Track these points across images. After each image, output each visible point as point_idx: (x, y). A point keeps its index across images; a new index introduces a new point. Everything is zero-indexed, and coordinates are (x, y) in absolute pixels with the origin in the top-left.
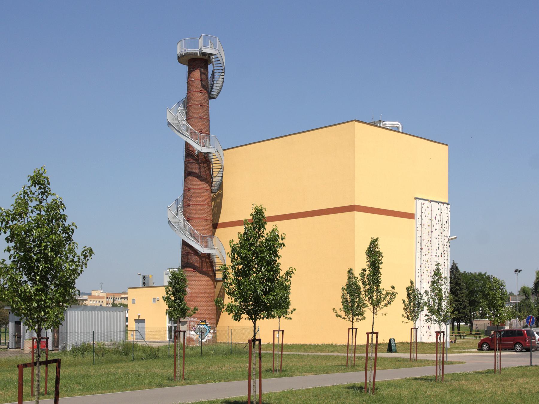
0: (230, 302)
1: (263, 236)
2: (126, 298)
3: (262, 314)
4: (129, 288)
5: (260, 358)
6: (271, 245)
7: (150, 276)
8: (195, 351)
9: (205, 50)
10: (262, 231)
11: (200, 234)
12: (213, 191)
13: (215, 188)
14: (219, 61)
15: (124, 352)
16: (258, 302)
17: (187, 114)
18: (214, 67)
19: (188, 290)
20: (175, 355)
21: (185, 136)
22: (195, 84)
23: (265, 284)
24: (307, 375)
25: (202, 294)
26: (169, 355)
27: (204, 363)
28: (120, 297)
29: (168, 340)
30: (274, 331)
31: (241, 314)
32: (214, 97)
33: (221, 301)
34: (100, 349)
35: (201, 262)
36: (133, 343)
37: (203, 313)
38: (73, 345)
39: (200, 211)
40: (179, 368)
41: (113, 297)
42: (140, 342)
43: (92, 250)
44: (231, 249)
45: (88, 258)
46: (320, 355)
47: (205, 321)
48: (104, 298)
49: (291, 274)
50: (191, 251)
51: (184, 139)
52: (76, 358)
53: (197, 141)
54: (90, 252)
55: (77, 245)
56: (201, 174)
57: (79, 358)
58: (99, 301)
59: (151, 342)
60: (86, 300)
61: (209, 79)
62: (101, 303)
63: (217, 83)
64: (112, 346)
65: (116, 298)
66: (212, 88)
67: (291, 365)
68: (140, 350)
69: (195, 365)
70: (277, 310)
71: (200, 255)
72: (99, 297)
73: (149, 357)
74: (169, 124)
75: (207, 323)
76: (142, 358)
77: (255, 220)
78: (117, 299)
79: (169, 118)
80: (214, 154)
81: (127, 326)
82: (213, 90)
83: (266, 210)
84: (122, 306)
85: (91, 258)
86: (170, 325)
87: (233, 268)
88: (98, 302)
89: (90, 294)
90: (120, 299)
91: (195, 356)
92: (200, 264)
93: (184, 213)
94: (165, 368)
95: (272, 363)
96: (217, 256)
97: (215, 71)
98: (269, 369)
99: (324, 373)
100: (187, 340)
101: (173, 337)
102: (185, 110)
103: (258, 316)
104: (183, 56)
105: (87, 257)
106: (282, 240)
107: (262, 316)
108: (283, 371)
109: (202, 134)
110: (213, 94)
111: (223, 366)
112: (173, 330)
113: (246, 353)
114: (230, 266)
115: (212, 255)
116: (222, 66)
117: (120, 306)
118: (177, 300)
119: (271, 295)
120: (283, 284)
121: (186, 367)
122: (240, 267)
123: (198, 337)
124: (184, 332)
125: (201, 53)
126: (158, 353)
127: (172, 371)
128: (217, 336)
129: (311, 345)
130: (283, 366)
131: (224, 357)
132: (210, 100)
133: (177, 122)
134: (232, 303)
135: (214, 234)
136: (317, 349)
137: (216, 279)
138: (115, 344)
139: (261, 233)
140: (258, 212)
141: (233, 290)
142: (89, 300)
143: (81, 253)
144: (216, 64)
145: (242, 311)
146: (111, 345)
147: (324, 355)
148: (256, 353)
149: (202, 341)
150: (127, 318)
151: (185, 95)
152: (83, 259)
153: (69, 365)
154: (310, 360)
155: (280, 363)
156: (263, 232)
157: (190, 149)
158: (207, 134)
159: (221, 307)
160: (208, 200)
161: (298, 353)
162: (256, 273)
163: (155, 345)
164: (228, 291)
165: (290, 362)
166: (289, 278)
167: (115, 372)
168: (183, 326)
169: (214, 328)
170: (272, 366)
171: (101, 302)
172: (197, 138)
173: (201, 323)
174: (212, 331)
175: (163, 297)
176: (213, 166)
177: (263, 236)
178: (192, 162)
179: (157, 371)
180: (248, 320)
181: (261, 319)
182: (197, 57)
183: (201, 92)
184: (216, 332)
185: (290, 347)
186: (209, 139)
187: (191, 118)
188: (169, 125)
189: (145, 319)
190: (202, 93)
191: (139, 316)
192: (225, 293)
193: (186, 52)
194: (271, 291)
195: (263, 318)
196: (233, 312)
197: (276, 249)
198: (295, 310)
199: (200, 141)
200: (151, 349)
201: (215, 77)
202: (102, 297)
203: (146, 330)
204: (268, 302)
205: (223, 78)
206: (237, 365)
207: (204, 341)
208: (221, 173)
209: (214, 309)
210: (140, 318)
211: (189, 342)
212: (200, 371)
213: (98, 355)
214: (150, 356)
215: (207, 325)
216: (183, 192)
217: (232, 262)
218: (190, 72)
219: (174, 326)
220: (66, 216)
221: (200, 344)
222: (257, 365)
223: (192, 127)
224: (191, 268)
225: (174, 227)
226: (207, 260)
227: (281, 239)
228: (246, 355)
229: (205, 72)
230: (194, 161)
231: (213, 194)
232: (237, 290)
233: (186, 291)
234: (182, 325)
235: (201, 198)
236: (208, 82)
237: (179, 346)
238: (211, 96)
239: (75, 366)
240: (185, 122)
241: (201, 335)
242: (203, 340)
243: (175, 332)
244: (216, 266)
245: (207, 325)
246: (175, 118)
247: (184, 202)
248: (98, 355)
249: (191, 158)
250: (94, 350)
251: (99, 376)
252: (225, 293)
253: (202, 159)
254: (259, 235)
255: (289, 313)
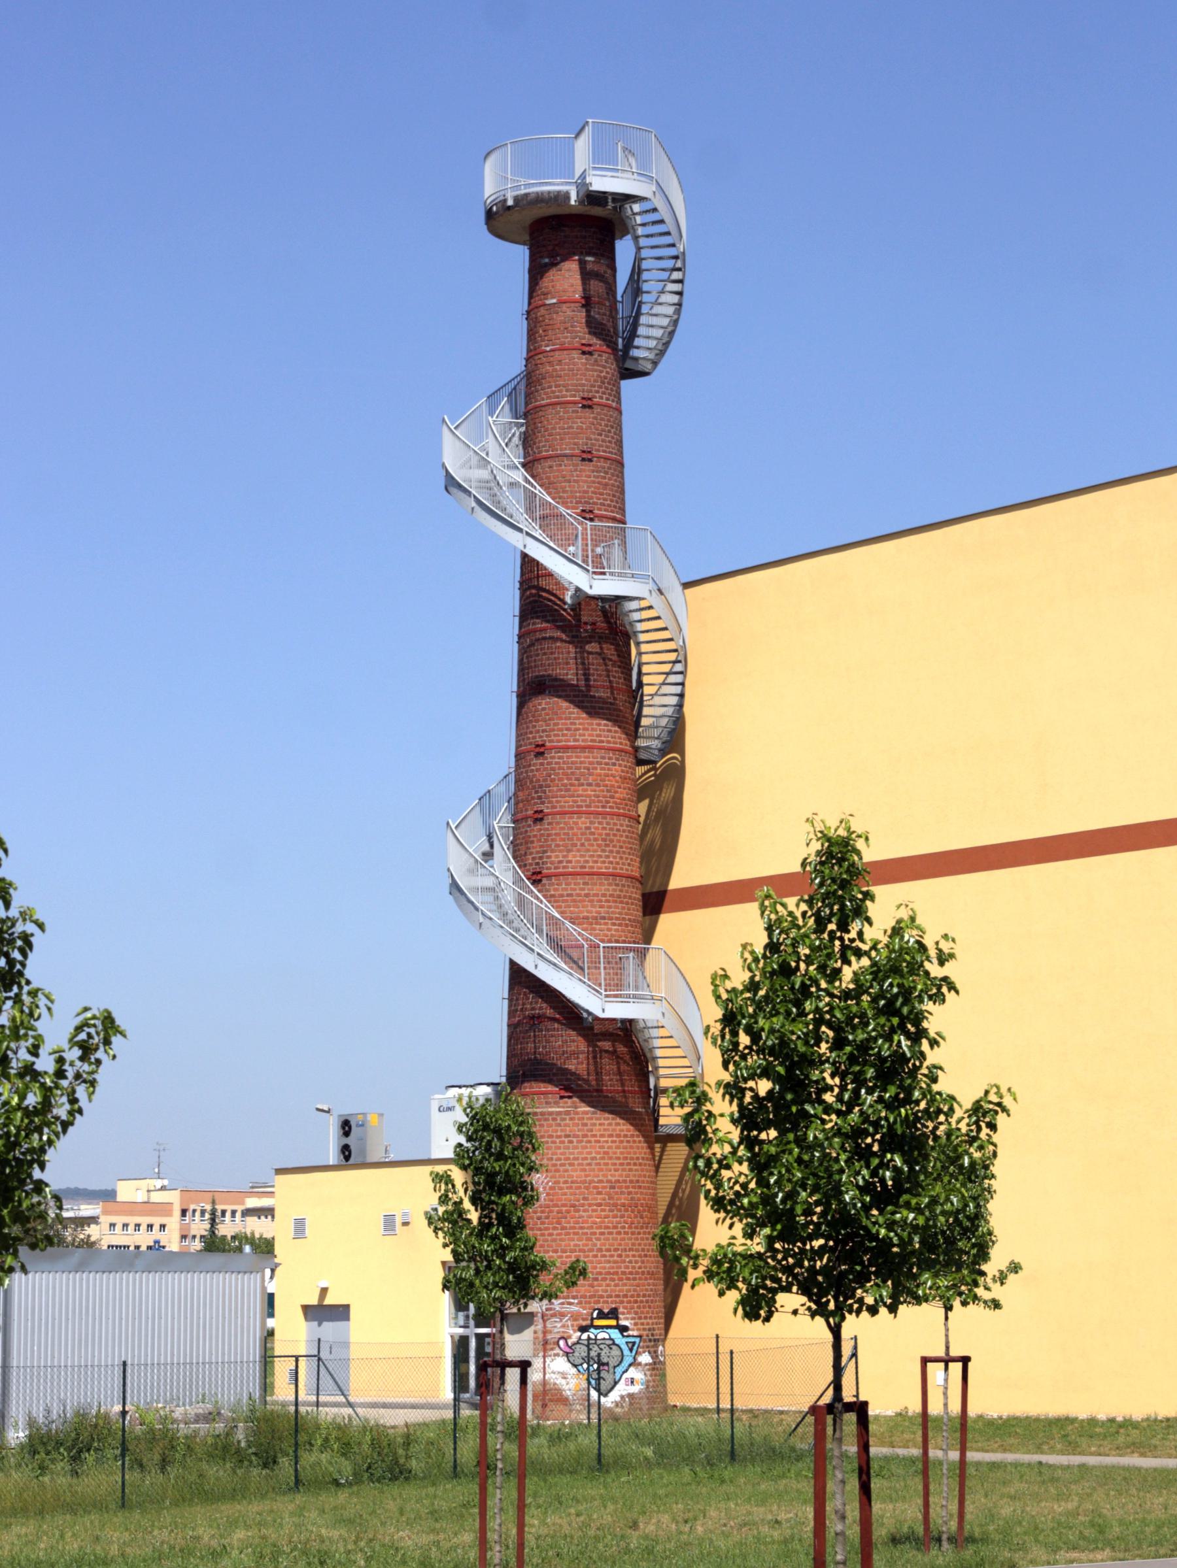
0: (724, 1242)
1: (859, 953)
2: (268, 1212)
3: (866, 1291)
4: (280, 1171)
5: (865, 1490)
6: (895, 990)
7: (373, 1119)
8: (572, 1446)
9: (602, 183)
10: (857, 929)
11: (587, 940)
12: (643, 756)
13: (649, 742)
14: (662, 222)
15: (255, 1454)
16: (849, 1237)
17: (527, 441)
18: (639, 249)
19: (538, 1179)
20: (485, 1465)
21: (520, 530)
22: (558, 318)
23: (875, 1162)
24: (1080, 1561)
25: (599, 1193)
26: (455, 1467)
27: (614, 1500)
28: (239, 1208)
29: (451, 1396)
30: (925, 1361)
31: (774, 1291)
32: (640, 368)
33: (683, 1236)
34: (152, 1437)
35: (595, 1058)
36: (297, 1411)
37: (604, 1279)
38: (31, 1423)
39: (589, 840)
40: (501, 1524)
41: (208, 1207)
42: (326, 1405)
43: (113, 1021)
44: (719, 1013)
45: (100, 1054)
46: (1139, 1469)
47: (614, 1314)
48: (169, 1213)
49: (996, 1113)
50: (549, 1012)
51: (514, 543)
52: (46, 1479)
53: (572, 549)
54: (105, 1029)
55: (52, 1002)
56: (588, 686)
57: (59, 1478)
58: (150, 1227)
59: (374, 1405)
60: (93, 1220)
61: (619, 298)
62: (156, 1234)
63: (654, 311)
64: (203, 1427)
65: (224, 1213)
66: (633, 334)
67: (1006, 1511)
68: (326, 1440)
69: (572, 1511)
70: (936, 1275)
71: (592, 1028)
72: (148, 1207)
73: (366, 1475)
74: (451, 483)
75: (623, 1323)
76: (338, 1477)
77: (821, 884)
78: (228, 1214)
79: (453, 457)
80: (644, 604)
81: (271, 1333)
82: (637, 342)
83: (867, 839)
84: (247, 1249)
85: (114, 1057)
86: (461, 1331)
87: (734, 1090)
88: (143, 1228)
89: (108, 1196)
90: (238, 1215)
91: (571, 1468)
92: (592, 1067)
93: (519, 851)
94: (438, 1526)
95: (920, 1501)
96: (662, 1032)
97: (645, 265)
98: (905, 1530)
99: (1162, 1552)
100: (535, 1396)
101: (472, 1383)
102: (519, 425)
103: (850, 1302)
104: (509, 208)
105: (96, 1049)
106: (942, 963)
107: (869, 1300)
108: (971, 1540)
109: (591, 520)
110: (636, 359)
111: (695, 1519)
112: (472, 1354)
113: (799, 1458)
114: (719, 1084)
115: (642, 1025)
116: (673, 245)
117: (240, 1249)
118: (490, 1225)
119: (907, 1205)
120: (960, 1157)
121: (533, 1521)
122: (764, 1086)
123: (584, 1384)
124: (524, 1366)
125: (581, 194)
126: (407, 1457)
127: (468, 1537)
128: (668, 1378)
129: (1092, 1422)
130: (968, 1517)
131: (701, 1474)
132: (625, 384)
133: (484, 474)
134: (730, 1244)
135: (648, 937)
136: (1121, 1439)
137: (662, 1131)
138: (219, 1414)
139: (852, 940)
140: (835, 849)
141: (737, 1188)
142: (105, 1220)
143: (69, 1036)
144: (647, 236)
145: (778, 1281)
146: (198, 1419)
147: (1155, 1470)
148: (847, 1457)
149: (603, 1399)
150: (271, 1297)
151: (515, 365)
152: (78, 1063)
153: (14, 1512)
154: (1094, 1489)
155: (956, 1501)
156: (860, 934)
157: (543, 583)
158: (614, 519)
159: (684, 1261)
160: (622, 793)
161: (1036, 1458)
162: (839, 1113)
163: (395, 1419)
164: (713, 1193)
165: (1002, 1496)
166: (985, 1131)
167: (214, 1543)
168: (516, 1337)
169: (654, 1341)
170: (920, 1517)
171: (156, 1228)
172: (571, 540)
173: (597, 1323)
174: (645, 1358)
175: (426, 1213)
176: (640, 654)
177: (859, 953)
178: (551, 638)
179: (402, 1538)
180: (804, 1319)
181: (865, 1314)
182: (566, 211)
183: (587, 349)
184: (663, 1363)
185: (998, 1428)
186: (624, 543)
187: (546, 458)
188: (453, 490)
189: (347, 1307)
190: (590, 353)
191: (324, 1291)
192: (703, 1202)
193: (523, 192)
194: (908, 1191)
195: (873, 1311)
196: (740, 1285)
197: (914, 1008)
198: (1015, 1268)
199: (585, 550)
200: (379, 1438)
201: (645, 287)
202: (164, 1209)
203: (354, 1353)
204: (895, 1240)
205: (680, 293)
206: (759, 1512)
207: (608, 1401)
208: (678, 678)
209: (654, 1263)
210: (328, 1301)
211: (544, 1406)
212: (597, 1539)
213: (141, 1466)
214: (369, 1467)
215: (623, 1329)
216: (513, 763)
217: (725, 1065)
218: (537, 273)
219: (478, 1336)
220: (10, 884)
221: (594, 1416)
222: (853, 1512)
223: (549, 494)
224: (550, 1082)
225: (477, 909)
226: (621, 1049)
227: (935, 961)
228: (800, 1465)
229: (602, 268)
230: (558, 634)
231: (644, 768)
232: (752, 1185)
233: (532, 1189)
234: (512, 1332)
235: (590, 785)
236: (613, 308)
237: (499, 1428)
238: (629, 364)
239: (41, 1513)
240: (519, 476)
241: (595, 1375)
242: (606, 1395)
243: (482, 1368)
244: (662, 1072)
245: (623, 1329)
246: (475, 459)
247: (516, 804)
248: (141, 1466)
249: (548, 621)
250: (123, 1443)
251: (145, 1560)
252: (703, 1202)
253: (593, 624)
254: (844, 948)
255: (989, 1280)
